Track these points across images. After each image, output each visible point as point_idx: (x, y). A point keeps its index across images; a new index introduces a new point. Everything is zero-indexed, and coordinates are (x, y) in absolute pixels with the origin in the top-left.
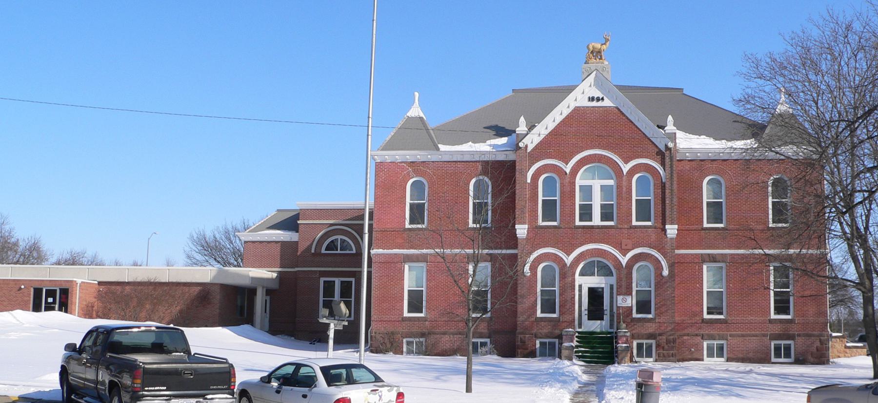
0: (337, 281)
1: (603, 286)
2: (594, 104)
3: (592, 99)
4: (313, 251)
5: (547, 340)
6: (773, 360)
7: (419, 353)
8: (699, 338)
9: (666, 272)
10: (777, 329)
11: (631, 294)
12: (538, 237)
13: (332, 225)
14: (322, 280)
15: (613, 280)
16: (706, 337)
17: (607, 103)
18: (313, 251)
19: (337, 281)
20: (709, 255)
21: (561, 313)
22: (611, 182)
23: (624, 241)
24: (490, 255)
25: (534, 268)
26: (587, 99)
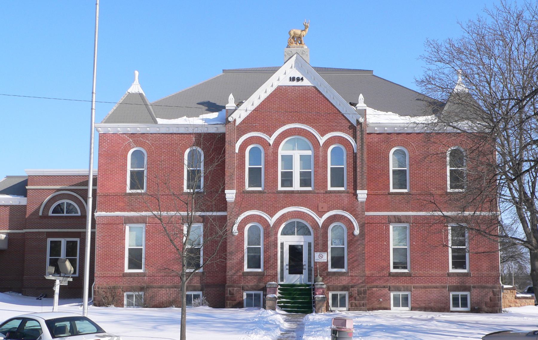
0: (63, 242)
1: (302, 244)
2: (295, 83)
3: (292, 79)
4: (40, 214)
5: (253, 292)
6: (452, 308)
7: (138, 305)
8: (387, 289)
9: (357, 232)
10: (455, 282)
11: (326, 251)
12: (245, 200)
13: (58, 190)
14: (49, 240)
15: (311, 239)
16: (392, 289)
17: (306, 83)
18: (40, 214)
19: (63, 242)
20: (395, 216)
21: (266, 268)
22: (309, 153)
23: (321, 205)
24: (203, 217)
25: (241, 228)
26: (288, 79)
